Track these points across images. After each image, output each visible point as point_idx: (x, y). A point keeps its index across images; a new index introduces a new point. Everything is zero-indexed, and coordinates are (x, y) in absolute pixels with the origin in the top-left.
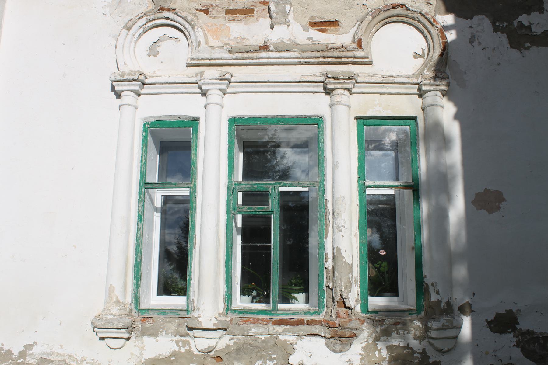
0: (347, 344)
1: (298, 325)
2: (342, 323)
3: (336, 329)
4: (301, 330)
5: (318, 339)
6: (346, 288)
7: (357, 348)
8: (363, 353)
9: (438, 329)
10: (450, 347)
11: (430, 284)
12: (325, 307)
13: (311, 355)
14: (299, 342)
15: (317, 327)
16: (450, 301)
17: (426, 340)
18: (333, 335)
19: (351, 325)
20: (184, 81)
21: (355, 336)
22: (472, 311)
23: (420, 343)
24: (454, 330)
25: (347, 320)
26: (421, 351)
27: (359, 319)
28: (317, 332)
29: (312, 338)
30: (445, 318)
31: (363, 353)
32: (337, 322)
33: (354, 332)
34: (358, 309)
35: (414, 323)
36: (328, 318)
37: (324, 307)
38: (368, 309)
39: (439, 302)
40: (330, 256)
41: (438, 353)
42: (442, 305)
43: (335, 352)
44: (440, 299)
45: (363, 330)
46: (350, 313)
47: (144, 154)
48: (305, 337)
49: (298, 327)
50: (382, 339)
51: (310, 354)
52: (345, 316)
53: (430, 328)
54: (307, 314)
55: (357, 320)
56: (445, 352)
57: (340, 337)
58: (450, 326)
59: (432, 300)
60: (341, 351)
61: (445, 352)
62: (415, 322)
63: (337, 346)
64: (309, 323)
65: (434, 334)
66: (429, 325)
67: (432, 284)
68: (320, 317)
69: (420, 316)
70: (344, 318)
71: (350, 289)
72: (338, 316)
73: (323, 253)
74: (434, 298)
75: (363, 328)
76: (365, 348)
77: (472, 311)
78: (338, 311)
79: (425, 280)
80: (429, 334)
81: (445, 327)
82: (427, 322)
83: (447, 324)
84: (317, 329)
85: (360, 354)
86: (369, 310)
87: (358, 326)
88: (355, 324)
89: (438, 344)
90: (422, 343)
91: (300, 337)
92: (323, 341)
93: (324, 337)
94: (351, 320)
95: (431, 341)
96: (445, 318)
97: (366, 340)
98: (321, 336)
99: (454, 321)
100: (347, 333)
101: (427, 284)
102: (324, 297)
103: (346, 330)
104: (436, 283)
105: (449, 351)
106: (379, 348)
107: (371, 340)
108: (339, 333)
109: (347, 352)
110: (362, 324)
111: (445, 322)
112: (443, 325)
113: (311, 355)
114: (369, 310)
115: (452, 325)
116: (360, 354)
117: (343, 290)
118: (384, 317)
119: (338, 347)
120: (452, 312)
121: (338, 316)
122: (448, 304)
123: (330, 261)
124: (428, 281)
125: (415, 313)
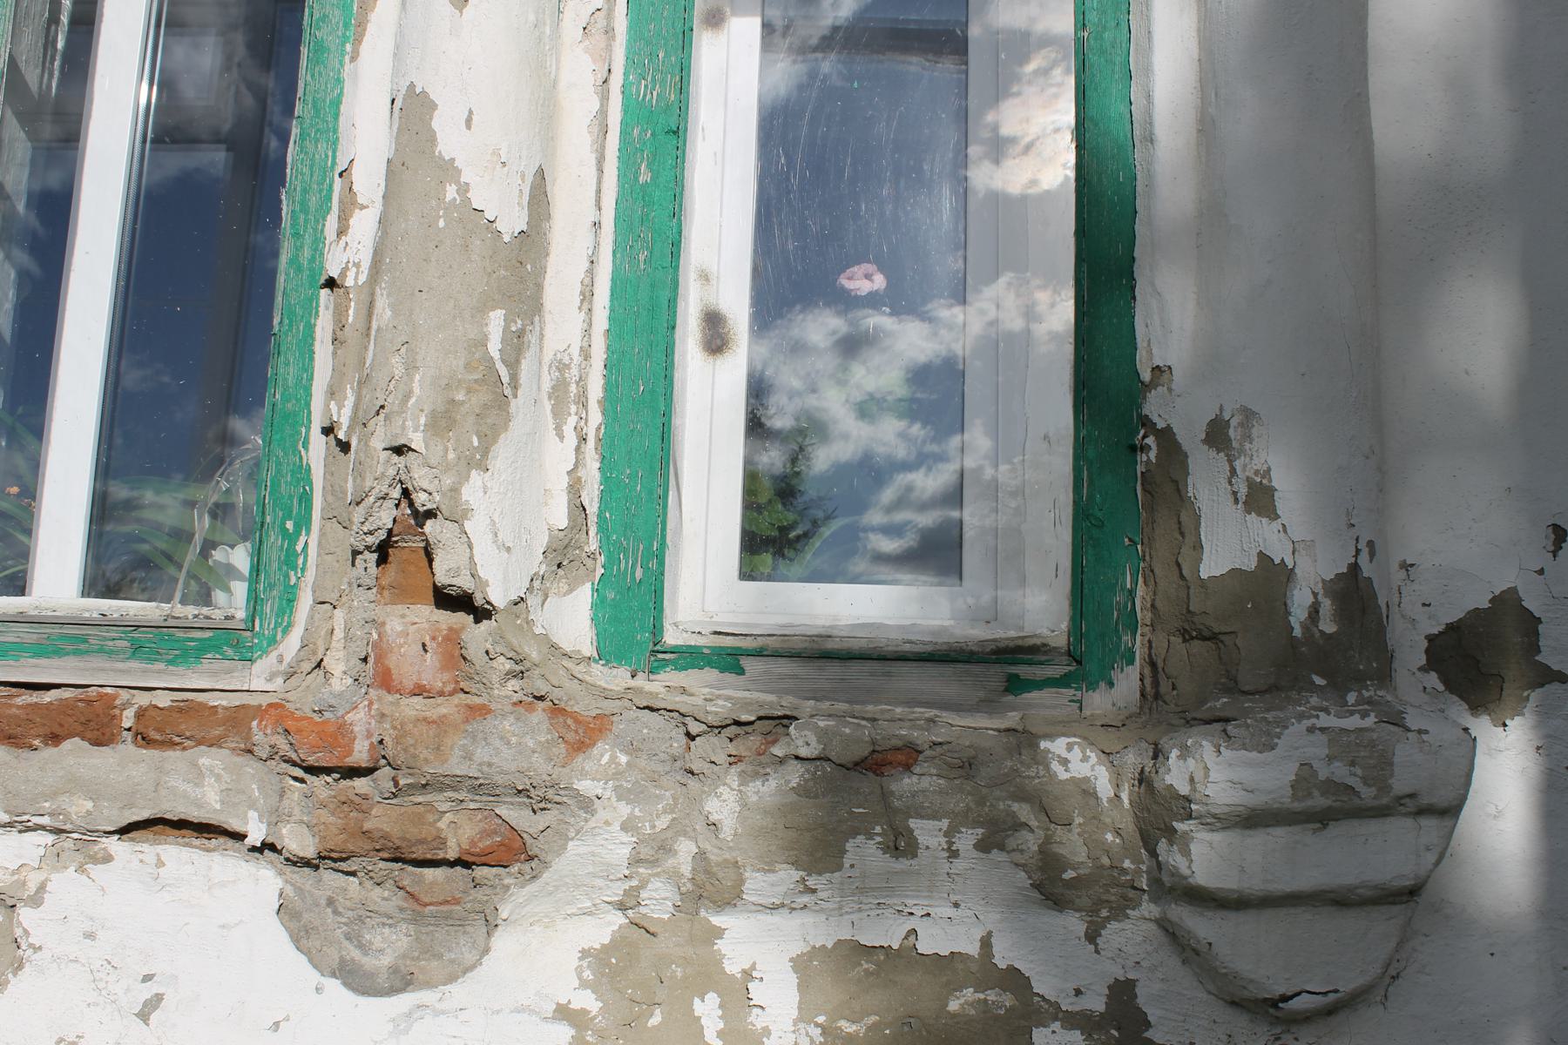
0: (461, 923)
1: (55, 739)
2: (402, 733)
3: (361, 784)
4: (74, 785)
5: (222, 863)
6: (442, 422)
7: (542, 950)
8: (587, 1001)
9: (1251, 820)
10: (1347, 986)
11: (1190, 436)
12: (305, 601)
13: (155, 1001)
14: (67, 887)
15: (209, 759)
16: (1367, 569)
17: (1148, 909)
18: (336, 841)
19: (481, 754)
20: (900, 663)
21: (511, 853)
22: (1546, 676)
23: (1092, 937)
24: (1399, 829)
25: (445, 708)
26: (1096, 1003)
27: (557, 710)
28: (208, 803)
29: (177, 855)
30: (1325, 720)
31: (587, 1001)
32: (359, 719)
33: (515, 814)
34: (571, 618)
35: (1042, 760)
36: (304, 698)
37: (290, 600)
38: (657, 630)
39: (1271, 577)
40: (369, 181)
41: (1240, 1023)
42: (1300, 601)
43: (359, 981)
44: (1279, 551)
45: (587, 804)
46: (474, 651)
47: (760, 642)
48: (114, 844)
49: (49, 753)
50: (757, 885)
51: (147, 991)
52: (429, 670)
53: (1183, 806)
54: (154, 655)
55: (539, 714)
56: (1307, 1018)
57: (407, 852)
58: (1367, 793)
59: (1212, 567)
60: (401, 981)
61: (1307, 1018)
62: (1058, 746)
63: (377, 937)
64: (156, 732)
65: (1205, 857)
66: (1175, 775)
67: (1217, 435)
68: (260, 678)
69: (1099, 702)
70: (420, 691)
71: (488, 440)
72: (378, 673)
73: (326, 171)
74: (1225, 545)
75: (586, 786)
76: (607, 966)
77: (1546, 676)
78: (378, 624)
79: (1154, 406)
80: (1171, 856)
81: (1319, 801)
82: (1158, 754)
83: (1340, 771)
84: (204, 781)
85: (564, 1013)
86: (671, 638)
87: (540, 767)
88: (512, 745)
89: (1257, 953)
90: (1116, 935)
91: (78, 841)
92: (267, 881)
93: (268, 847)
94: (482, 711)
95: (1200, 925)
96: (1325, 720)
97: (616, 891)
98: (239, 837)
99: (1405, 753)
100: (458, 829)
101: (1166, 436)
102: (304, 522)
103: (441, 800)
104: (1249, 415)
105: (1336, 1009)
106: (733, 967)
107: (659, 901)
108: (382, 819)
109: (458, 992)
110: (581, 746)
111: (1316, 749)
112: (1304, 781)
113: (155, 1001)
114: (671, 638)
115: (1384, 788)
116: (564, 1013)
117: (416, 440)
118: (786, 704)
119: (389, 944)
120: (1384, 676)
121: (378, 673)
122: (1353, 593)
123: (364, 226)
124: (1179, 410)
125: (1063, 682)
